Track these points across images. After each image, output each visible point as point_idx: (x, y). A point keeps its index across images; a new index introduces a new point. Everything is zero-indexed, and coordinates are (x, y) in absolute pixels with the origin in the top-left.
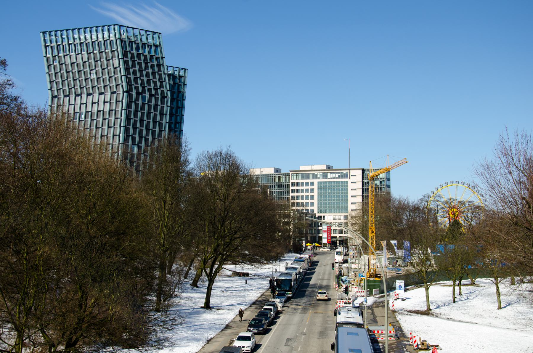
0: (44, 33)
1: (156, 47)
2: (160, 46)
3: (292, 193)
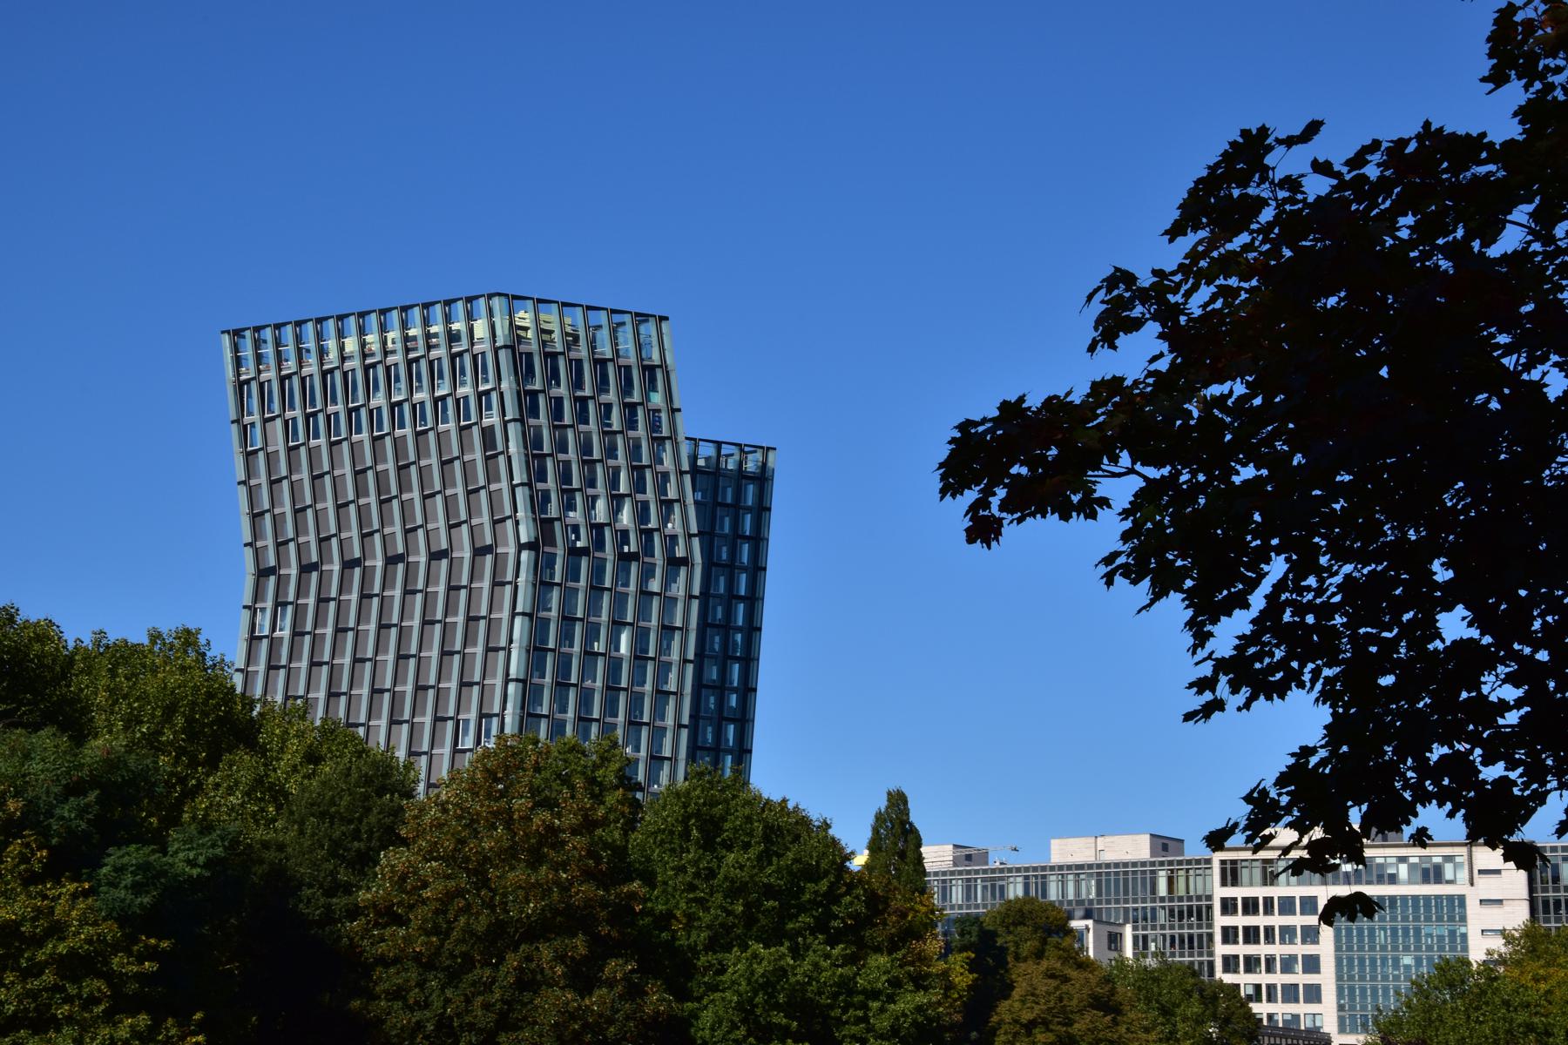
0: (237, 333)
1: (649, 370)
2: (663, 366)
3: (1225, 941)
